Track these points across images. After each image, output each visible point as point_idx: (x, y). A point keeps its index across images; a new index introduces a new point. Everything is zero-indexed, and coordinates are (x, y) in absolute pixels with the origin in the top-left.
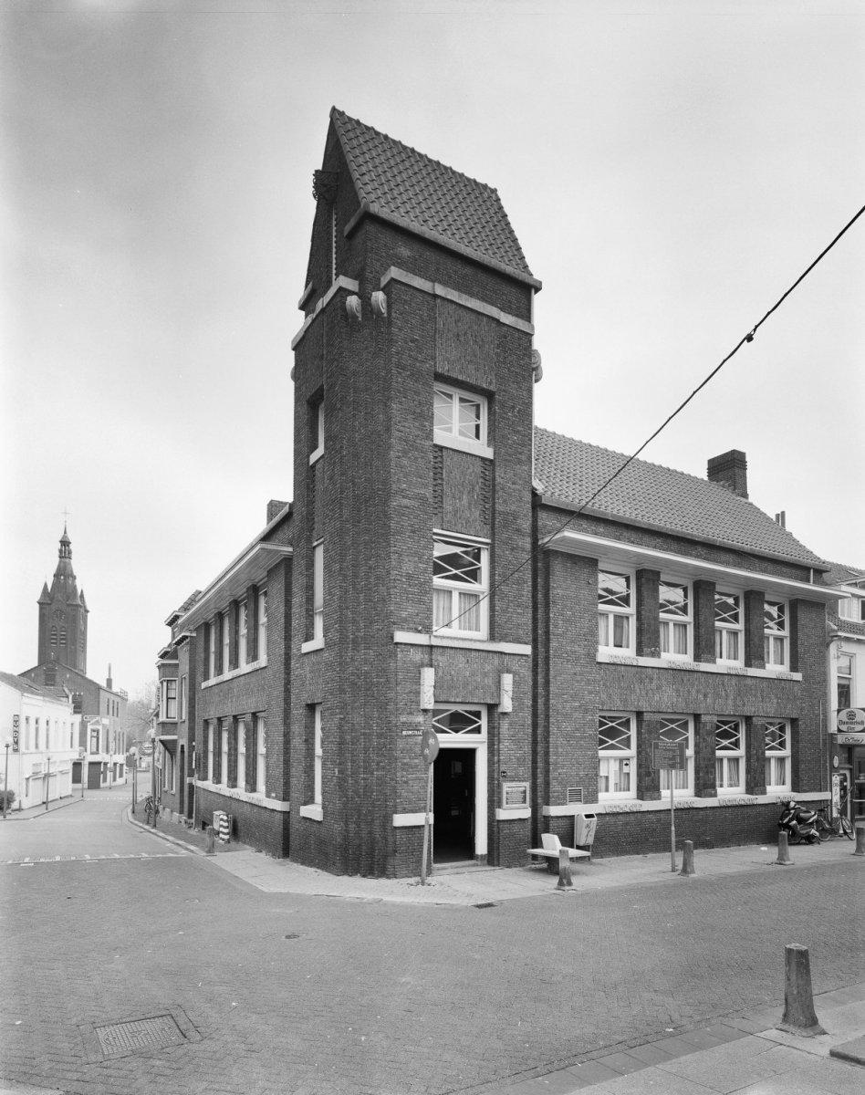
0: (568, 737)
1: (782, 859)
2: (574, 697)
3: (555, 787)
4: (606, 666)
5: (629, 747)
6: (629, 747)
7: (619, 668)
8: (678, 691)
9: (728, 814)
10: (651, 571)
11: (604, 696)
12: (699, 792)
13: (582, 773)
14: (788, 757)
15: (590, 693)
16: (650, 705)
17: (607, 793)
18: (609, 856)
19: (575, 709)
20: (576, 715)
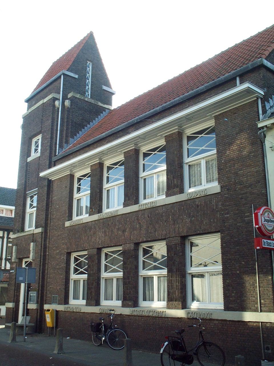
8: (105, 232)
13: (58, 288)
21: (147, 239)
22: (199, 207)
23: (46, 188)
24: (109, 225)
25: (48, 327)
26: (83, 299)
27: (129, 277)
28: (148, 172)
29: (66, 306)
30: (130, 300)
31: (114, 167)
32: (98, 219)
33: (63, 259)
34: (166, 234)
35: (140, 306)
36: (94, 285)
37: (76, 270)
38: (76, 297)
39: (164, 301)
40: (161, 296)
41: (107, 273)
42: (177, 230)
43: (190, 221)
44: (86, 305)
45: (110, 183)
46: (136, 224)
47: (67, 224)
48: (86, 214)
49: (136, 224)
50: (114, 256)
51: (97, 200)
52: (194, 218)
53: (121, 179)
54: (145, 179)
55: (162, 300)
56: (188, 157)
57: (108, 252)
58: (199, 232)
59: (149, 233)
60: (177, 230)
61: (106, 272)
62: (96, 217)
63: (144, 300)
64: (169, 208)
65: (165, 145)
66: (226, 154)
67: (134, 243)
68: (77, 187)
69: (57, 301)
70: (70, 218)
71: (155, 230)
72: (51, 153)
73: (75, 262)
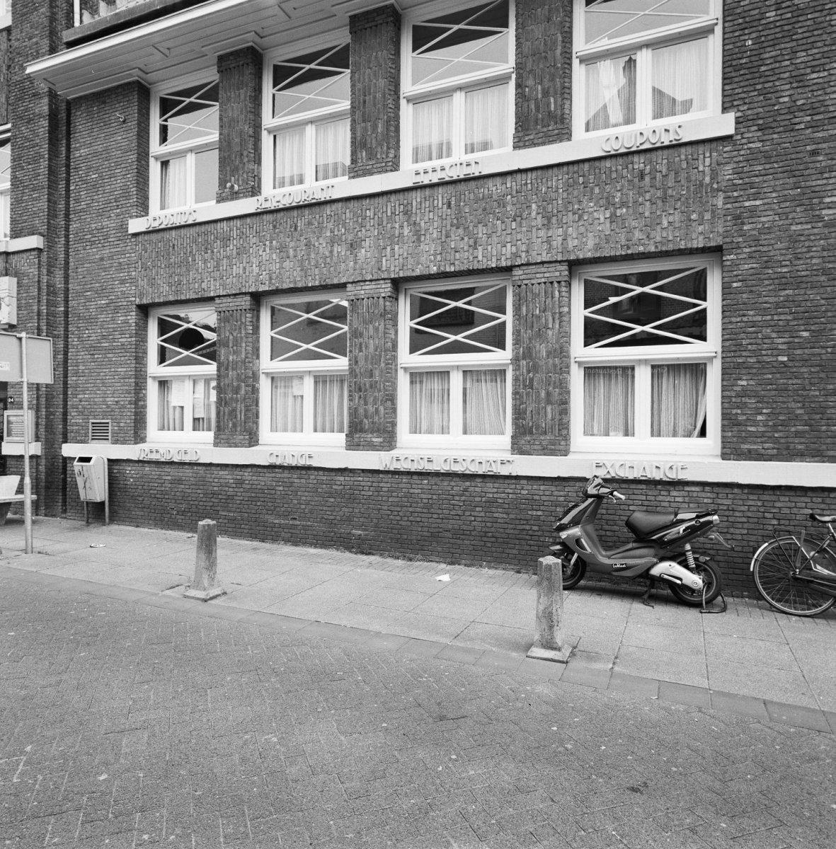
0: (93, 349)
1: (549, 619)
2: (100, 293)
3: (75, 419)
4: (146, 237)
5: (503, 347)
6: (503, 347)
7: (166, 235)
8: (282, 249)
9: (420, 488)
10: (231, 54)
11: (143, 283)
12: (525, 438)
13: (110, 400)
14: (711, 359)
15: (123, 282)
16: (224, 286)
17: (702, 440)
18: (149, 526)
19: (102, 309)
20: (102, 317)
21: (442, 269)
22: (647, 179)
23: (45, 123)
24: (296, 229)
25: (83, 502)
27: (371, 370)
28: (286, 118)
29: (141, 446)
31: (304, 68)
32: (255, 211)
33: (126, 322)
34: (516, 255)
36: (243, 392)
39: (341, 431)
40: (168, 419)
42: (557, 242)
43: (610, 217)
44: (216, 444)
45: (170, 144)
46: (401, 227)
48: (692, 100)
49: (401, 227)
51: (246, 160)
52: (624, 210)
56: (273, 118)
57: (165, 316)
58: (641, 249)
59: (453, 252)
60: (557, 242)
62: (246, 206)
63: (290, 426)
64: (529, 182)
65: (218, 84)
66: (764, 22)
67: (391, 279)
69: (110, 434)
70: (143, 207)
71: (475, 243)
72: (52, 19)
73: (418, 311)
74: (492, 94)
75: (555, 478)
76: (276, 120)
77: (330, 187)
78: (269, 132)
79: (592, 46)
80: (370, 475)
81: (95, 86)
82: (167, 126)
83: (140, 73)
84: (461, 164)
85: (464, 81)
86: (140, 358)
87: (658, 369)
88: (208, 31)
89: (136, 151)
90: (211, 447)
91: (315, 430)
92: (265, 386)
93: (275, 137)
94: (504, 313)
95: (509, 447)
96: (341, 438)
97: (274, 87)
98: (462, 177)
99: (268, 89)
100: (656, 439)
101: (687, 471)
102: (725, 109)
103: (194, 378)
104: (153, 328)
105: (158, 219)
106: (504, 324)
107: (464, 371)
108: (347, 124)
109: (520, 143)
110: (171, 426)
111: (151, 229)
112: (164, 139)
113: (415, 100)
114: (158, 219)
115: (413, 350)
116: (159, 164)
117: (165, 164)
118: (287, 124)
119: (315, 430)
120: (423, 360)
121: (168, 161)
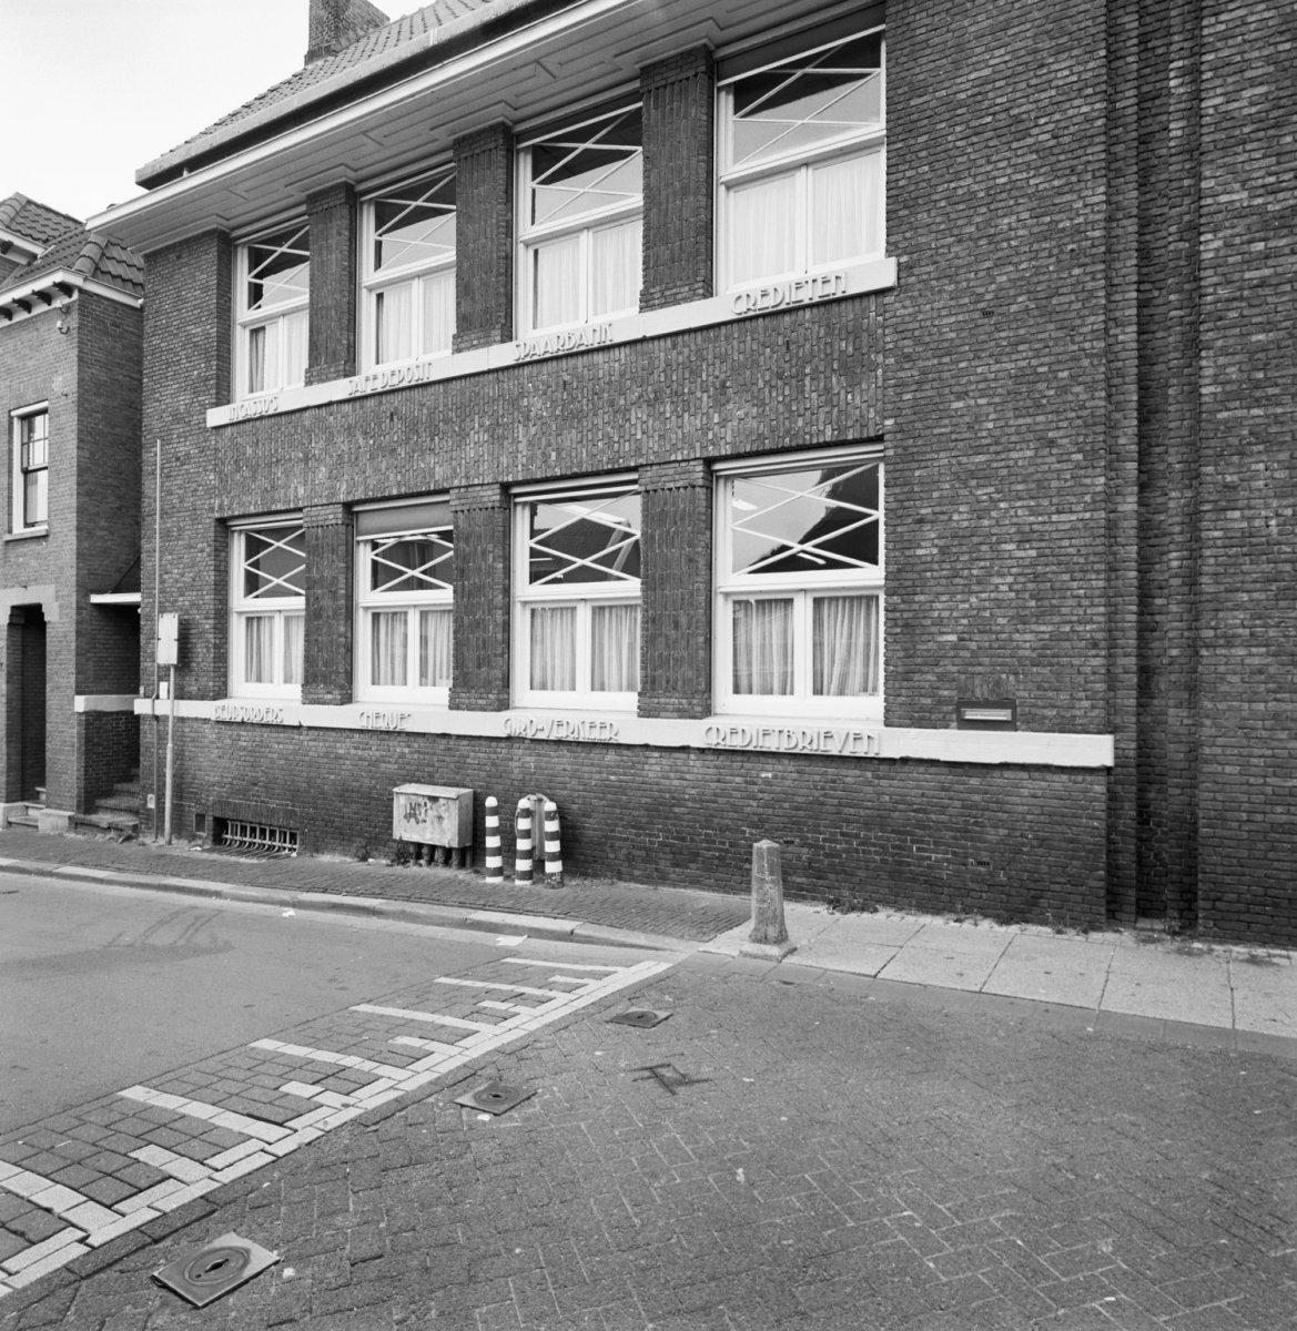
6: (875, 561)
26: (288, 679)
29: (505, 714)
30: (326, 680)
35: (238, 694)
37: (252, 584)
38: (257, 674)
39: (631, 688)
41: (257, 597)
47: (217, 417)
50: (277, 544)
53: (297, 294)
54: (380, 297)
55: (754, 689)
61: (255, 594)
62: (339, 389)
63: (597, 685)
68: (250, 283)
70: (223, 396)
74: (612, 236)
75: (438, 735)
76: (535, 228)
77: (820, 281)
78: (527, 246)
79: (741, 167)
80: (945, 770)
81: (160, 241)
82: (261, 286)
83: (219, 220)
84: (814, 281)
85: (813, 153)
86: (222, 587)
87: (599, 610)
88: (292, 167)
89: (1205, 32)
90: (299, 704)
91: (593, 689)
92: (521, 622)
93: (536, 252)
94: (876, 507)
95: (881, 717)
96: (631, 700)
97: (534, 178)
98: (816, 300)
99: (368, 233)
100: (818, 697)
101: (410, 719)
102: (889, 253)
103: (533, 606)
104: (238, 546)
105: (772, 292)
106: (876, 523)
107: (735, 602)
108: (880, 160)
109: (647, 303)
110: (557, 683)
111: (388, 388)
112: (378, 265)
113: (730, 186)
114: (772, 292)
115: (534, 577)
116: (247, 333)
117: (257, 332)
118: (841, 149)
119: (593, 689)
120: (543, 591)
121: (263, 328)
